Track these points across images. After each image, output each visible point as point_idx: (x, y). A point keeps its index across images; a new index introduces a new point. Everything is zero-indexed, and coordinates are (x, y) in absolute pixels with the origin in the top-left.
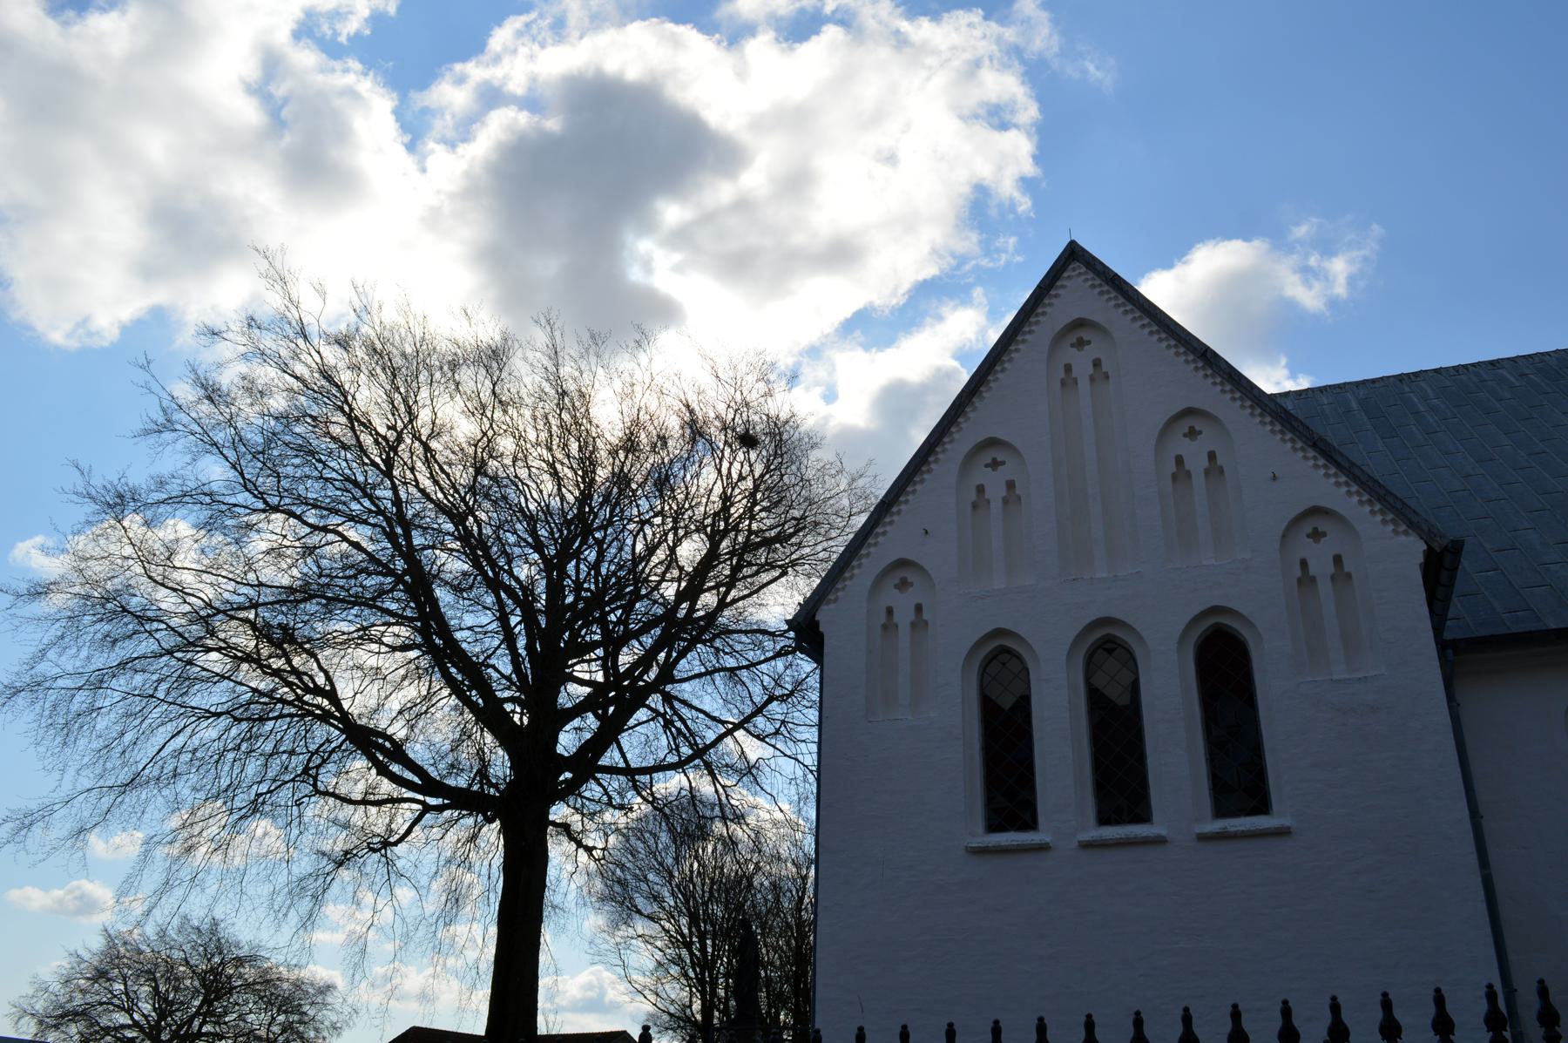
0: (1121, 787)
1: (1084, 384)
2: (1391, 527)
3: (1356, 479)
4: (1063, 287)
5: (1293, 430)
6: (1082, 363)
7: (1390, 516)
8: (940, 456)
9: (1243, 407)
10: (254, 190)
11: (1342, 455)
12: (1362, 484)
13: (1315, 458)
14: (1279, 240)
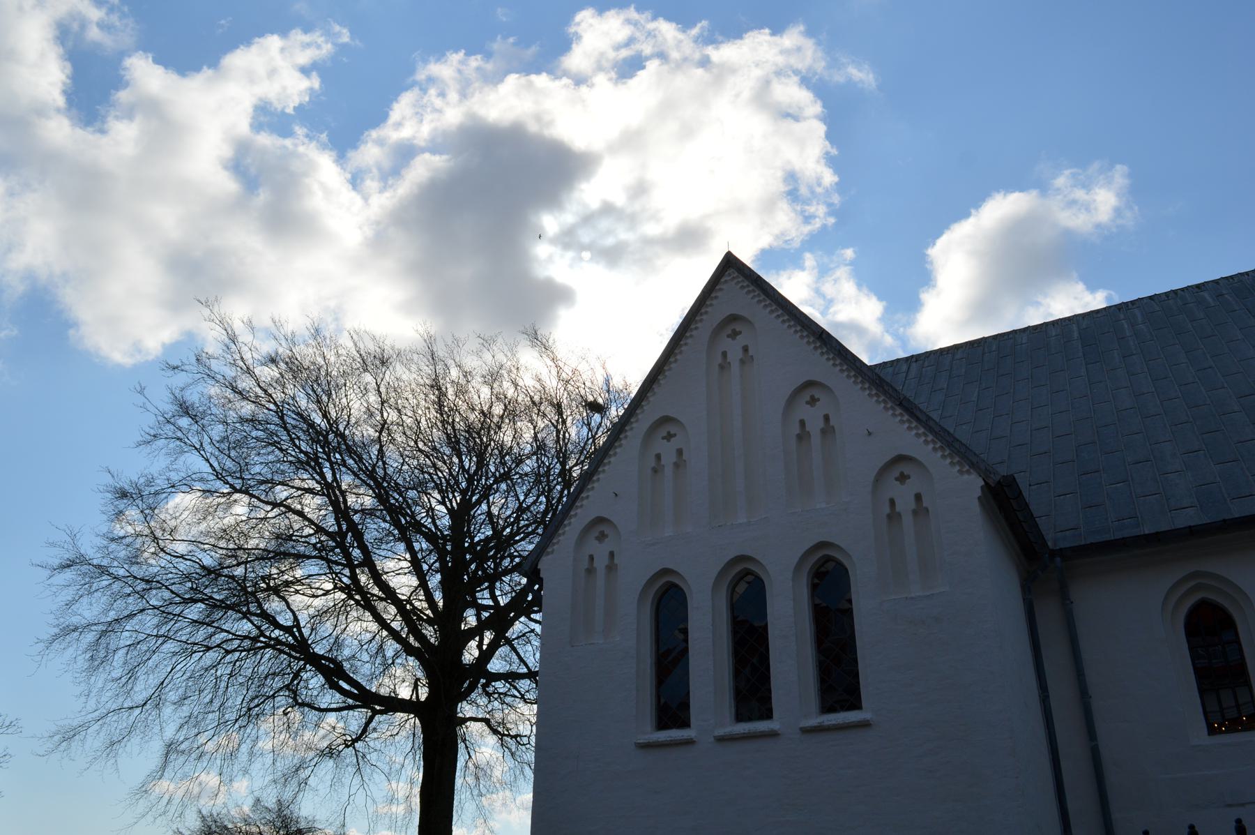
0: (752, 695)
1: (735, 367)
2: (958, 468)
3: (931, 430)
4: (721, 290)
5: (885, 393)
6: (734, 349)
7: (957, 459)
8: (628, 434)
9: (848, 377)
10: (244, 240)
11: (921, 411)
12: (935, 434)
13: (901, 415)
14: (1043, 187)
